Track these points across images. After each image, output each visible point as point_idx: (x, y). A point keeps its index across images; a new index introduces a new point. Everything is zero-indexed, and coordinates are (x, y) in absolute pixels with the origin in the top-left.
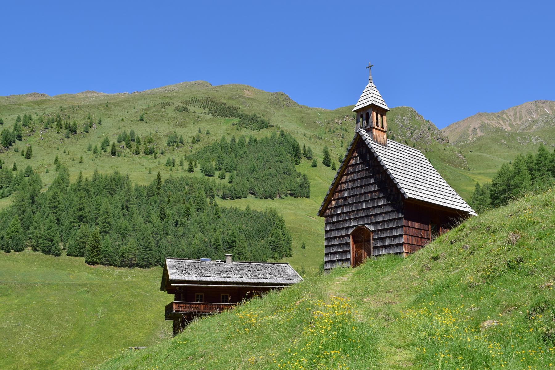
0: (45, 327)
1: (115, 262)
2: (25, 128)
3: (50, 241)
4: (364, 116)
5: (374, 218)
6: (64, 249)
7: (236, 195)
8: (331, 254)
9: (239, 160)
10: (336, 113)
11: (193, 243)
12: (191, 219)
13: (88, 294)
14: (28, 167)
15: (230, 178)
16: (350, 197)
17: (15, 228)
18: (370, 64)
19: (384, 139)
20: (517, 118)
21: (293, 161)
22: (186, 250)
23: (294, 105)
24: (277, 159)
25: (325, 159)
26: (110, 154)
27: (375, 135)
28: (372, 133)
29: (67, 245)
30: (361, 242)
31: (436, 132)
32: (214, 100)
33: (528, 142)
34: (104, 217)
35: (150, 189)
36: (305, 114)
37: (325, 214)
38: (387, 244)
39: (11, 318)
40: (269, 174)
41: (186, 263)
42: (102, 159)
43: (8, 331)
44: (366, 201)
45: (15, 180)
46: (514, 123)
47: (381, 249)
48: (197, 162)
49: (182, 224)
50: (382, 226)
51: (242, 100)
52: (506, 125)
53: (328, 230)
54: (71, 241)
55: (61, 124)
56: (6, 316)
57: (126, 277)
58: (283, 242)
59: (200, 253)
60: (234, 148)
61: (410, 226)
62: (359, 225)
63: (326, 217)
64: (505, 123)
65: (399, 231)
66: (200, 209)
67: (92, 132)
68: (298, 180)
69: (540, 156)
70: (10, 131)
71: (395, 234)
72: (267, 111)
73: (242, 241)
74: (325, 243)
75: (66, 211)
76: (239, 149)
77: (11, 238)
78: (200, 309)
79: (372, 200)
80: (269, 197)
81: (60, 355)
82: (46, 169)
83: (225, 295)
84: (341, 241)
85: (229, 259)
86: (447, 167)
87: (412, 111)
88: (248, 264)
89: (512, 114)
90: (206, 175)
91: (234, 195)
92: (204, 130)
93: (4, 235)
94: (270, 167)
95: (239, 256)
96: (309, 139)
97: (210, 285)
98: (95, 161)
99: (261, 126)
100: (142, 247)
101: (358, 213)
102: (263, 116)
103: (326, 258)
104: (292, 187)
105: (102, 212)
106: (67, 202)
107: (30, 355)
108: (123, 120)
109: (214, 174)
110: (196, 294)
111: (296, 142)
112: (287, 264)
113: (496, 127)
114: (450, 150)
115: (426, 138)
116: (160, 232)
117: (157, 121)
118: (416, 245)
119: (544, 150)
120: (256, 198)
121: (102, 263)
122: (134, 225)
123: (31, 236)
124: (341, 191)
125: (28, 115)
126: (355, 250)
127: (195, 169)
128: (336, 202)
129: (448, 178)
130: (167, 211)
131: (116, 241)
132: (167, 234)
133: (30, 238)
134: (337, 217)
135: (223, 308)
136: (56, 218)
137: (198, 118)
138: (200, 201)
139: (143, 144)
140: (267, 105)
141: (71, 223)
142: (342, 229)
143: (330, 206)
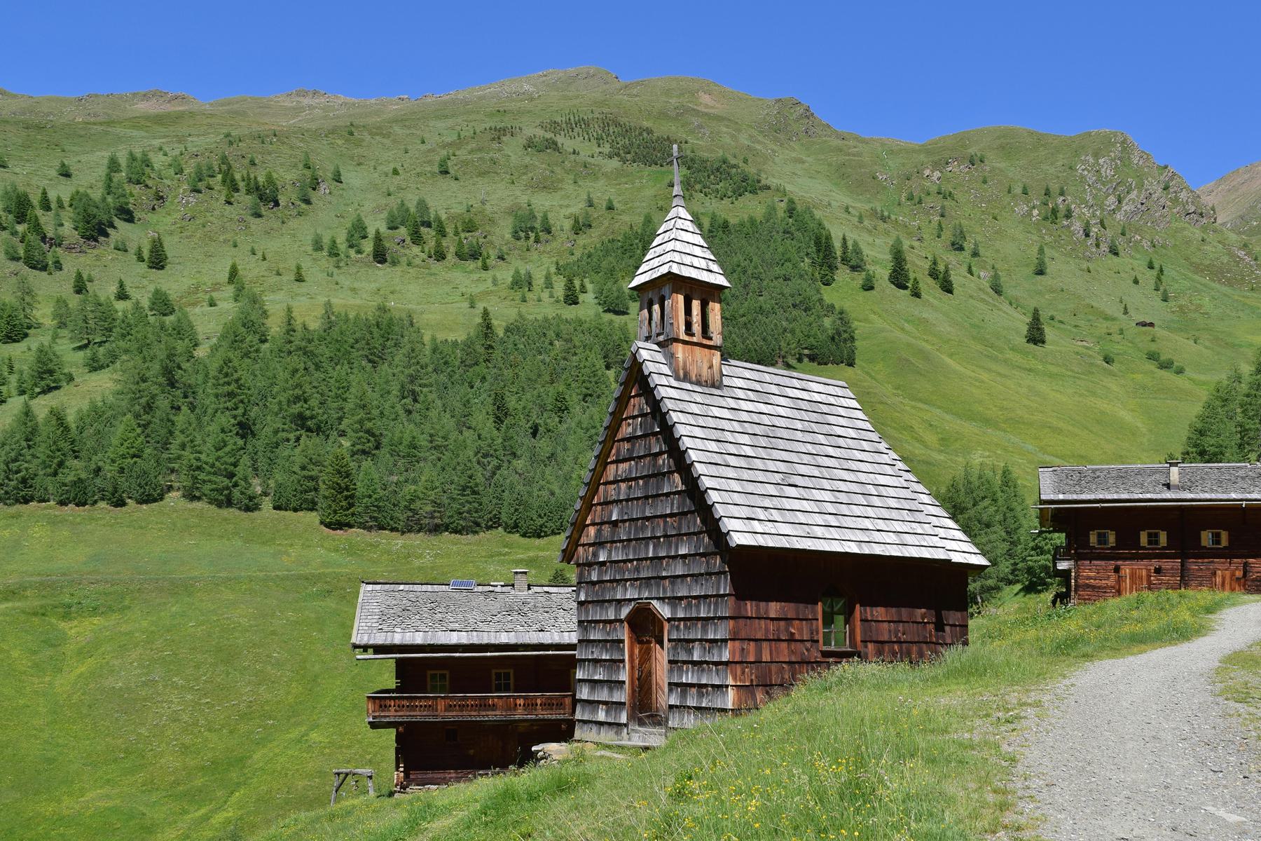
0: (223, 679)
1: (391, 522)
2: (136, 189)
3: (225, 477)
6: (265, 494)
10: (928, 152)
11: (574, 476)
13: (328, 599)
14: (157, 292)
16: (624, 521)
17: (128, 448)
19: (711, 367)
22: (557, 491)
23: (825, 133)
24: (778, 271)
25: (894, 271)
26: (371, 258)
27: (681, 360)
29: (272, 483)
31: (1183, 195)
32: (623, 120)
34: (357, 418)
35: (468, 344)
36: (849, 155)
38: (695, 659)
39: (131, 663)
40: (758, 309)
41: (411, 595)
42: (353, 270)
43: (126, 695)
45: (123, 325)
48: (586, 281)
49: (549, 431)
54: (279, 476)
55: (233, 180)
56: (120, 661)
57: (420, 556)
62: (642, 599)
66: (591, 395)
67: (321, 204)
68: (827, 322)
70: (92, 196)
71: (712, 637)
72: (756, 150)
75: (260, 404)
77: (122, 470)
78: (437, 711)
81: (261, 743)
82: (207, 297)
83: (502, 671)
84: (608, 634)
86: (1205, 285)
87: (1123, 142)
90: (608, 311)
92: (600, 199)
93: (100, 464)
94: (761, 292)
96: (857, 219)
97: (457, 655)
98: (335, 277)
100: (453, 486)
102: (746, 161)
104: (812, 339)
105: (352, 406)
106: (261, 383)
107: (187, 748)
108: (396, 172)
109: (627, 309)
110: (429, 673)
114: (1219, 242)
115: (1156, 212)
116: (496, 450)
117: (482, 174)
121: (363, 526)
122: (431, 435)
123: (176, 466)
125: (138, 152)
127: (581, 297)
129: (1207, 314)
130: (512, 402)
131: (391, 474)
132: (514, 455)
133: (173, 471)
135: (494, 705)
136: (236, 422)
137: (585, 167)
138: (589, 377)
139: (451, 235)
141: (276, 432)
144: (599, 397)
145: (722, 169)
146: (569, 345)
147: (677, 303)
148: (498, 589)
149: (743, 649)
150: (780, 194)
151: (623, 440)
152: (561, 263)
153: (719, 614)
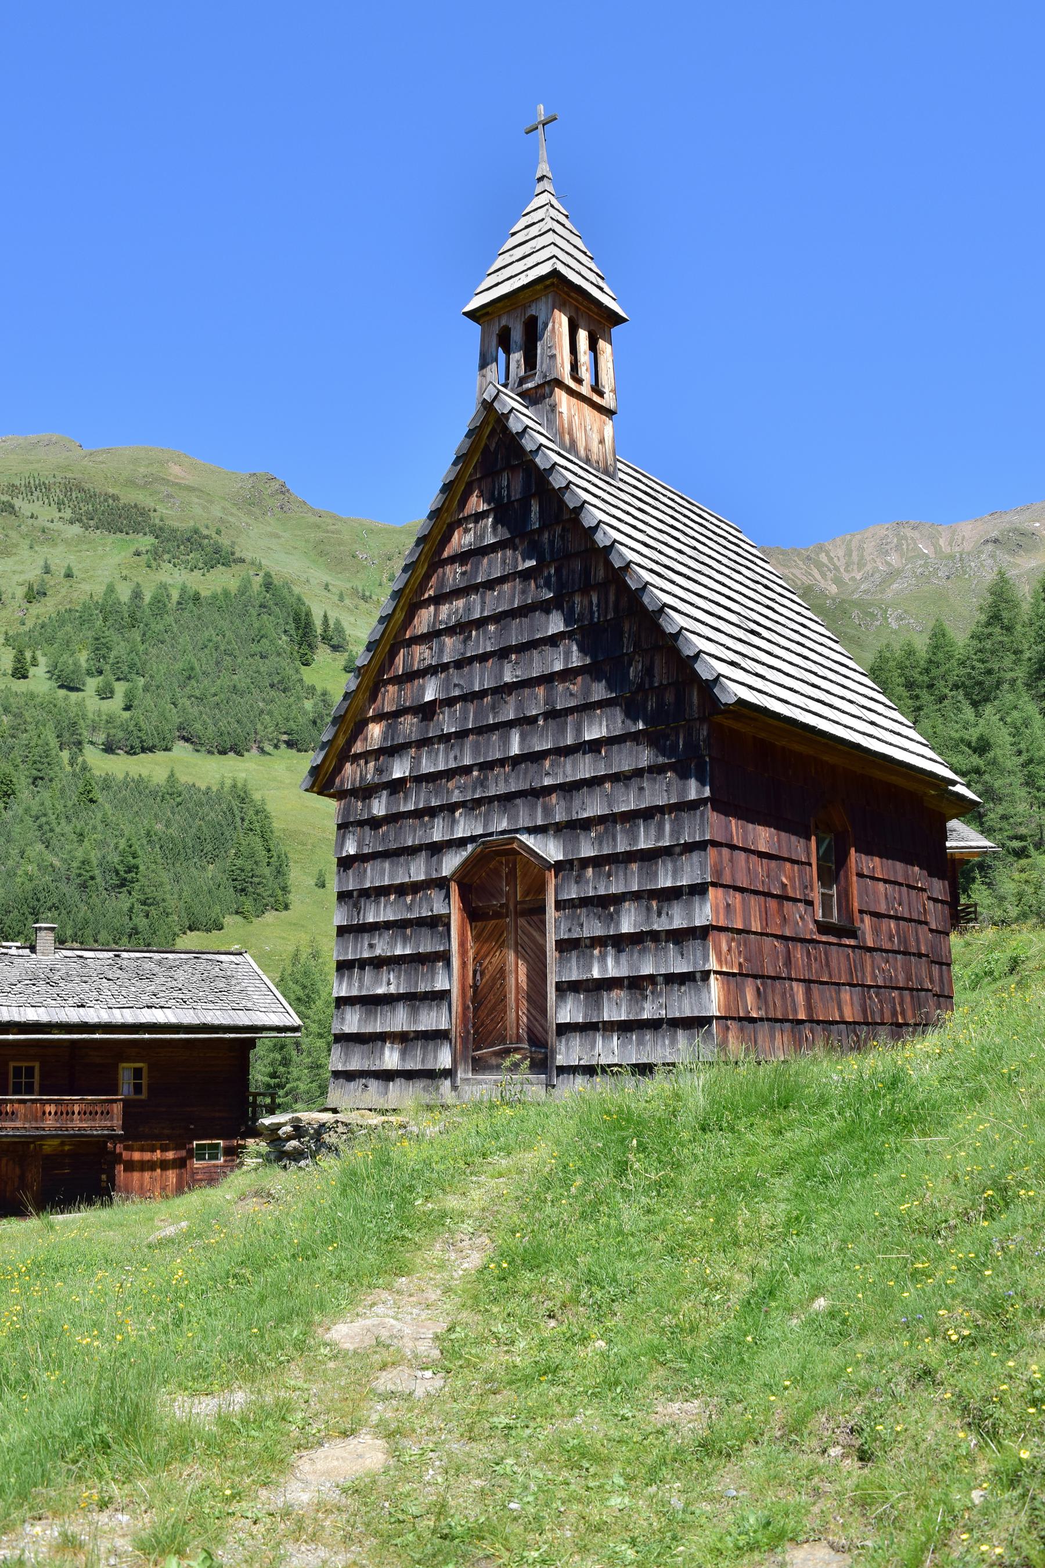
4: (517, 335)
5: (562, 803)
7: (141, 742)
8: (362, 968)
9: (151, 649)
11: (20, 872)
12: (15, 807)
15: (126, 695)
16: (450, 702)
18: (541, 112)
19: (602, 441)
20: (854, 563)
21: (295, 653)
24: (255, 648)
27: (565, 416)
28: (553, 408)
30: (498, 915)
32: (86, 486)
33: (878, 623)
36: (328, 532)
37: (338, 780)
44: (526, 722)
46: (846, 577)
47: (596, 952)
48: (39, 653)
50: (599, 839)
51: (163, 488)
52: (826, 580)
53: (349, 857)
58: (267, 871)
59: (38, 900)
60: (138, 615)
61: (735, 842)
62: (491, 834)
63: (340, 795)
64: (824, 576)
65: (687, 868)
66: (42, 778)
68: (308, 705)
69: (936, 648)
71: (669, 884)
73: (154, 866)
74: (339, 917)
76: (152, 619)
79: (552, 714)
80: (231, 749)
83: (24, 1064)
84: (410, 908)
85: (45, 940)
88: (111, 954)
89: (841, 553)
90: (61, 687)
91: (137, 743)
92: (59, 566)
95: (146, 908)
99: (212, 559)
101: (486, 778)
102: (218, 532)
103: (340, 983)
109: (84, 685)
111: (304, 604)
112: (241, 954)
113: (803, 584)
118: (762, 934)
119: (944, 635)
120: (197, 751)
124: (411, 676)
126: (471, 954)
127: (32, 671)
128: (389, 726)
134: (391, 794)
135: (13, 1113)
137: (44, 532)
140: (228, 505)
142: (412, 851)
143: (358, 748)
144: (51, 780)
145: (192, 540)
146: (19, 721)
147: (560, 325)
148: (13, 951)
149: (728, 905)
150: (255, 568)
151: (453, 559)
152: (11, 633)
153: (686, 838)
